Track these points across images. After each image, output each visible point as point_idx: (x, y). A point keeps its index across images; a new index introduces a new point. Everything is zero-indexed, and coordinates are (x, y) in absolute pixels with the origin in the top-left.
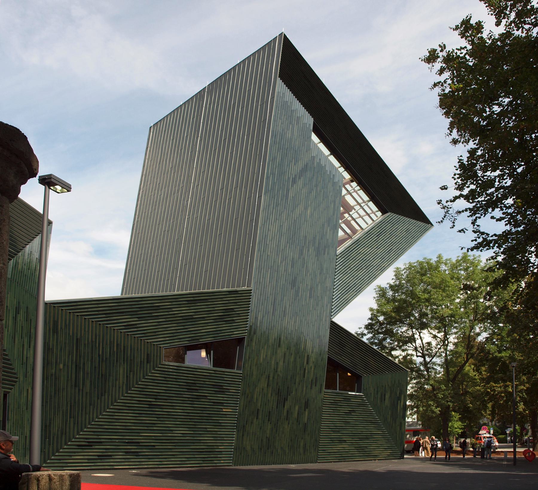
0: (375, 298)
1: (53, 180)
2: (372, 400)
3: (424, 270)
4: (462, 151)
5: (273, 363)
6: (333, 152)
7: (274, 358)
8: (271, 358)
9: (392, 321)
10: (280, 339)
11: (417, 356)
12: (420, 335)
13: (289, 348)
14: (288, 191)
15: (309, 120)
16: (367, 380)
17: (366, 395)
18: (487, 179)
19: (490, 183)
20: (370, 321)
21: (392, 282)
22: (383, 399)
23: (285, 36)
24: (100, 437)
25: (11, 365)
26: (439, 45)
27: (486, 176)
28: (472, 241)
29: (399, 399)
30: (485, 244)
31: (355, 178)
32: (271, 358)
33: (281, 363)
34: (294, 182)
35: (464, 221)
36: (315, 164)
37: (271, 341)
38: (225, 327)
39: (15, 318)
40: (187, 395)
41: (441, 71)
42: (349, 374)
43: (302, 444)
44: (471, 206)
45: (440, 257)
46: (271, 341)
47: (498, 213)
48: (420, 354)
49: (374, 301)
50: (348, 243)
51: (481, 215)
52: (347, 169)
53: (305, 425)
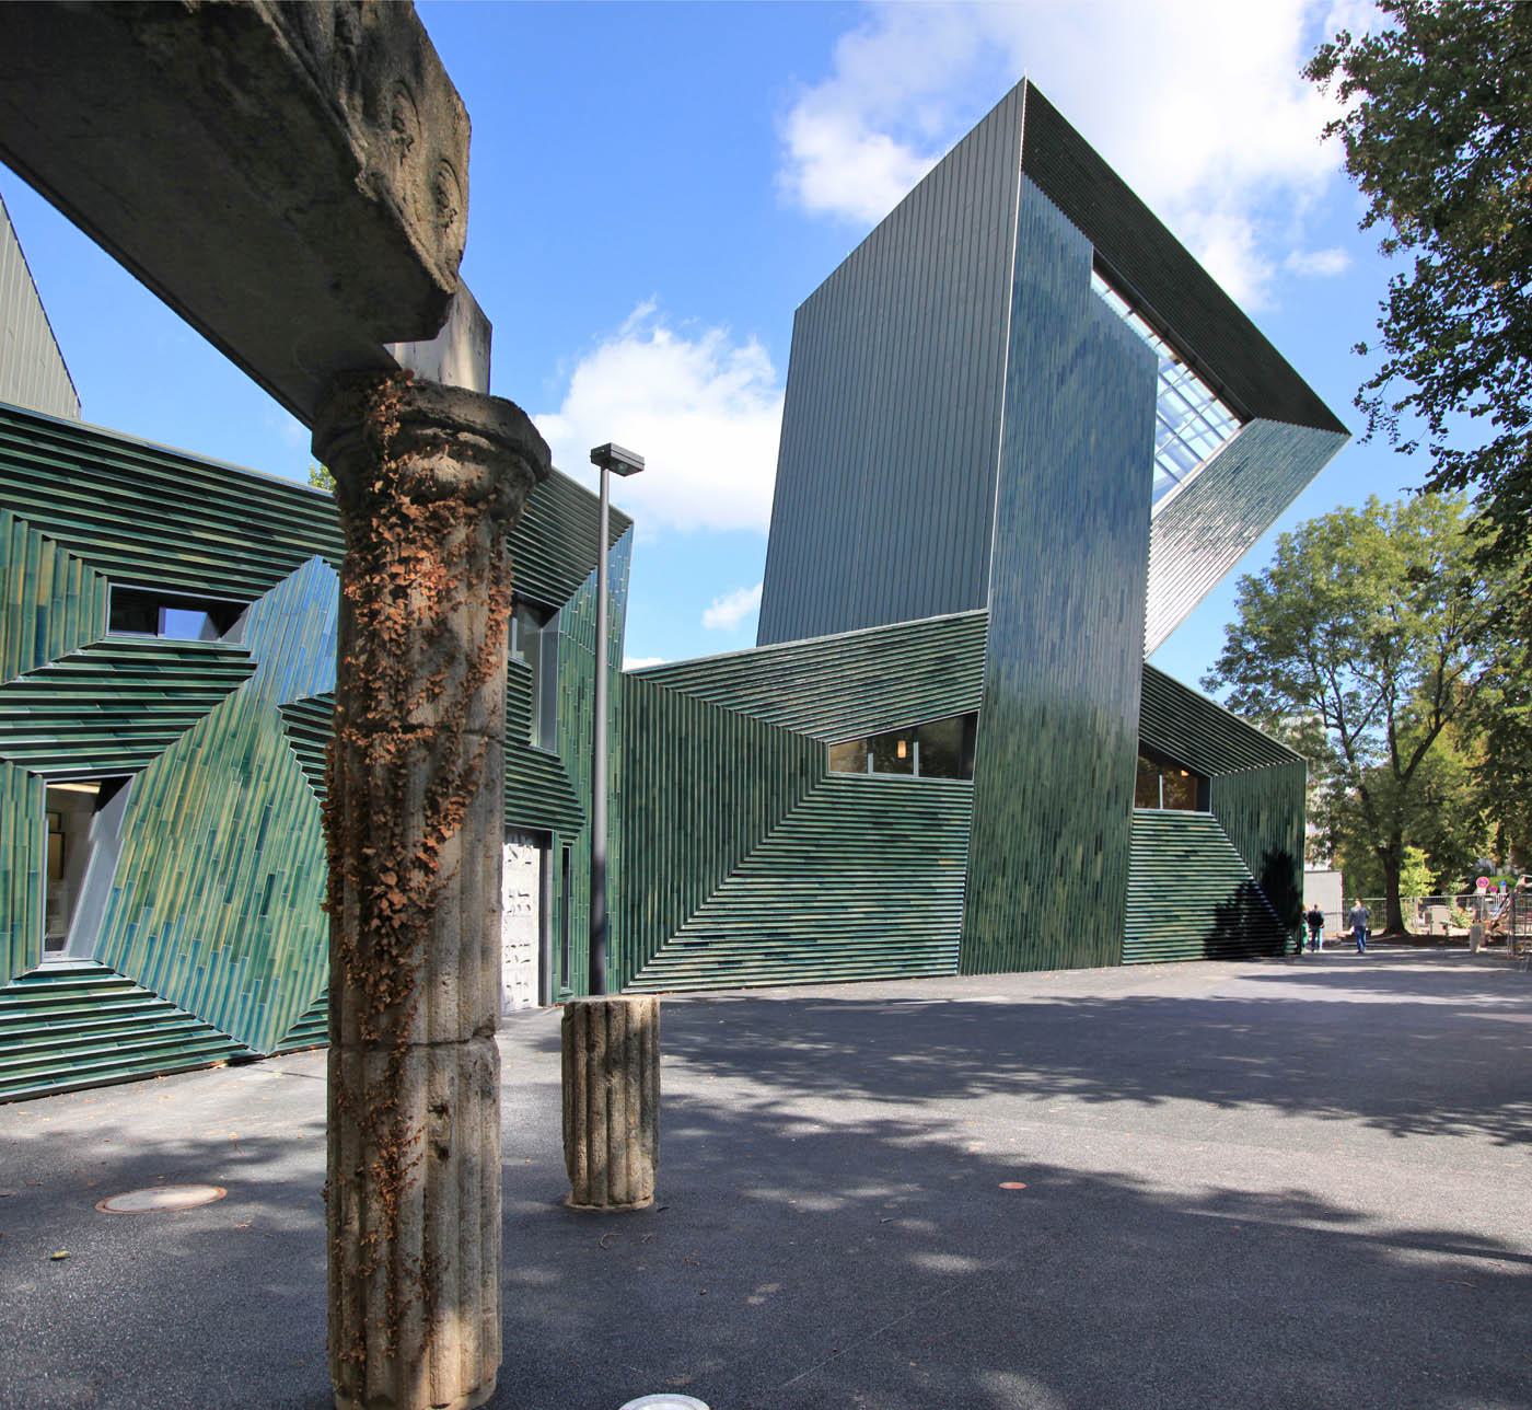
0: (1237, 602)
1: (613, 454)
2: (1232, 826)
3: (1337, 534)
4: (1405, 264)
5: (1032, 759)
6: (1135, 306)
7: (1033, 750)
8: (1028, 752)
9: (1281, 647)
10: (1044, 708)
11: (1327, 726)
12: (1332, 679)
13: (1061, 728)
14: (1050, 402)
15: (1086, 248)
16: (1222, 781)
17: (1219, 815)
18: (1452, 323)
19: (1460, 331)
20: (1226, 654)
21: (1274, 567)
22: (1254, 824)
23: (1031, 88)
24: (722, 926)
25: (573, 794)
26: (1338, 37)
27: (1449, 317)
28: (1428, 476)
29: (1288, 822)
30: (1452, 474)
31: (1182, 355)
32: (1028, 752)
33: (1048, 761)
34: (1062, 380)
35: (1413, 424)
36: (1101, 337)
37: (1027, 715)
38: (937, 693)
39: (578, 709)
40: (873, 835)
41: (1346, 90)
42: (1184, 773)
43: (1091, 927)
44: (1419, 390)
45: (1372, 502)
46: (1027, 715)
47: (1480, 396)
48: (1334, 721)
49: (1237, 609)
50: (1177, 490)
51: (1444, 407)
52: (1166, 337)
53: (1098, 886)
